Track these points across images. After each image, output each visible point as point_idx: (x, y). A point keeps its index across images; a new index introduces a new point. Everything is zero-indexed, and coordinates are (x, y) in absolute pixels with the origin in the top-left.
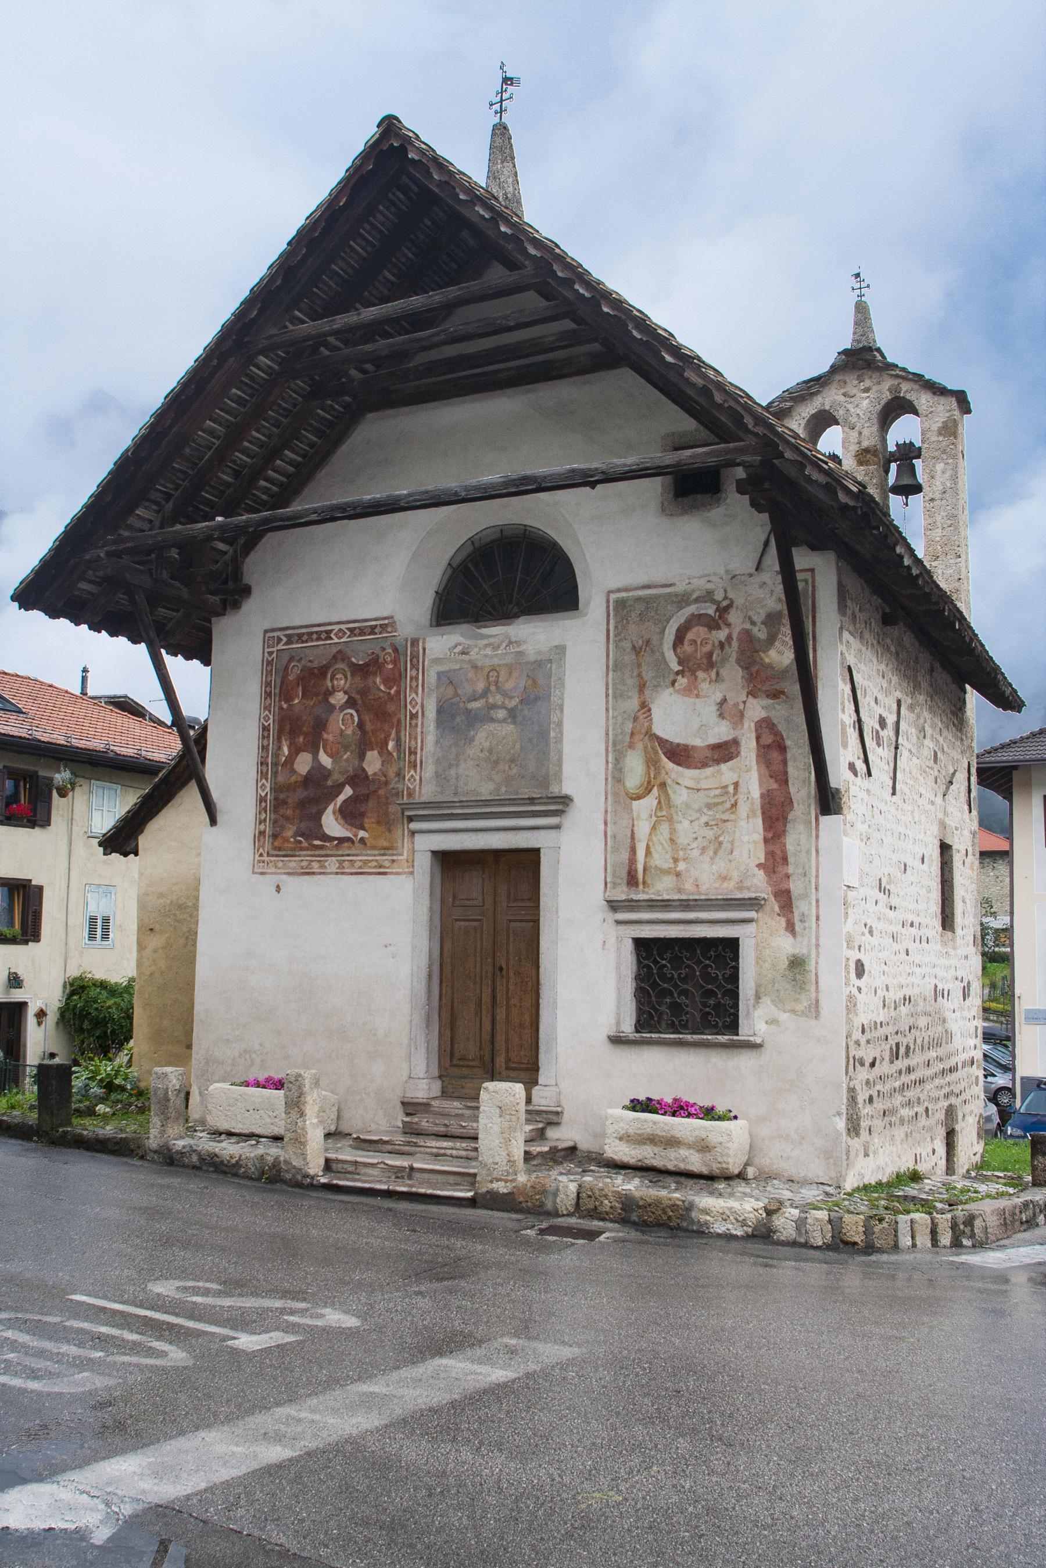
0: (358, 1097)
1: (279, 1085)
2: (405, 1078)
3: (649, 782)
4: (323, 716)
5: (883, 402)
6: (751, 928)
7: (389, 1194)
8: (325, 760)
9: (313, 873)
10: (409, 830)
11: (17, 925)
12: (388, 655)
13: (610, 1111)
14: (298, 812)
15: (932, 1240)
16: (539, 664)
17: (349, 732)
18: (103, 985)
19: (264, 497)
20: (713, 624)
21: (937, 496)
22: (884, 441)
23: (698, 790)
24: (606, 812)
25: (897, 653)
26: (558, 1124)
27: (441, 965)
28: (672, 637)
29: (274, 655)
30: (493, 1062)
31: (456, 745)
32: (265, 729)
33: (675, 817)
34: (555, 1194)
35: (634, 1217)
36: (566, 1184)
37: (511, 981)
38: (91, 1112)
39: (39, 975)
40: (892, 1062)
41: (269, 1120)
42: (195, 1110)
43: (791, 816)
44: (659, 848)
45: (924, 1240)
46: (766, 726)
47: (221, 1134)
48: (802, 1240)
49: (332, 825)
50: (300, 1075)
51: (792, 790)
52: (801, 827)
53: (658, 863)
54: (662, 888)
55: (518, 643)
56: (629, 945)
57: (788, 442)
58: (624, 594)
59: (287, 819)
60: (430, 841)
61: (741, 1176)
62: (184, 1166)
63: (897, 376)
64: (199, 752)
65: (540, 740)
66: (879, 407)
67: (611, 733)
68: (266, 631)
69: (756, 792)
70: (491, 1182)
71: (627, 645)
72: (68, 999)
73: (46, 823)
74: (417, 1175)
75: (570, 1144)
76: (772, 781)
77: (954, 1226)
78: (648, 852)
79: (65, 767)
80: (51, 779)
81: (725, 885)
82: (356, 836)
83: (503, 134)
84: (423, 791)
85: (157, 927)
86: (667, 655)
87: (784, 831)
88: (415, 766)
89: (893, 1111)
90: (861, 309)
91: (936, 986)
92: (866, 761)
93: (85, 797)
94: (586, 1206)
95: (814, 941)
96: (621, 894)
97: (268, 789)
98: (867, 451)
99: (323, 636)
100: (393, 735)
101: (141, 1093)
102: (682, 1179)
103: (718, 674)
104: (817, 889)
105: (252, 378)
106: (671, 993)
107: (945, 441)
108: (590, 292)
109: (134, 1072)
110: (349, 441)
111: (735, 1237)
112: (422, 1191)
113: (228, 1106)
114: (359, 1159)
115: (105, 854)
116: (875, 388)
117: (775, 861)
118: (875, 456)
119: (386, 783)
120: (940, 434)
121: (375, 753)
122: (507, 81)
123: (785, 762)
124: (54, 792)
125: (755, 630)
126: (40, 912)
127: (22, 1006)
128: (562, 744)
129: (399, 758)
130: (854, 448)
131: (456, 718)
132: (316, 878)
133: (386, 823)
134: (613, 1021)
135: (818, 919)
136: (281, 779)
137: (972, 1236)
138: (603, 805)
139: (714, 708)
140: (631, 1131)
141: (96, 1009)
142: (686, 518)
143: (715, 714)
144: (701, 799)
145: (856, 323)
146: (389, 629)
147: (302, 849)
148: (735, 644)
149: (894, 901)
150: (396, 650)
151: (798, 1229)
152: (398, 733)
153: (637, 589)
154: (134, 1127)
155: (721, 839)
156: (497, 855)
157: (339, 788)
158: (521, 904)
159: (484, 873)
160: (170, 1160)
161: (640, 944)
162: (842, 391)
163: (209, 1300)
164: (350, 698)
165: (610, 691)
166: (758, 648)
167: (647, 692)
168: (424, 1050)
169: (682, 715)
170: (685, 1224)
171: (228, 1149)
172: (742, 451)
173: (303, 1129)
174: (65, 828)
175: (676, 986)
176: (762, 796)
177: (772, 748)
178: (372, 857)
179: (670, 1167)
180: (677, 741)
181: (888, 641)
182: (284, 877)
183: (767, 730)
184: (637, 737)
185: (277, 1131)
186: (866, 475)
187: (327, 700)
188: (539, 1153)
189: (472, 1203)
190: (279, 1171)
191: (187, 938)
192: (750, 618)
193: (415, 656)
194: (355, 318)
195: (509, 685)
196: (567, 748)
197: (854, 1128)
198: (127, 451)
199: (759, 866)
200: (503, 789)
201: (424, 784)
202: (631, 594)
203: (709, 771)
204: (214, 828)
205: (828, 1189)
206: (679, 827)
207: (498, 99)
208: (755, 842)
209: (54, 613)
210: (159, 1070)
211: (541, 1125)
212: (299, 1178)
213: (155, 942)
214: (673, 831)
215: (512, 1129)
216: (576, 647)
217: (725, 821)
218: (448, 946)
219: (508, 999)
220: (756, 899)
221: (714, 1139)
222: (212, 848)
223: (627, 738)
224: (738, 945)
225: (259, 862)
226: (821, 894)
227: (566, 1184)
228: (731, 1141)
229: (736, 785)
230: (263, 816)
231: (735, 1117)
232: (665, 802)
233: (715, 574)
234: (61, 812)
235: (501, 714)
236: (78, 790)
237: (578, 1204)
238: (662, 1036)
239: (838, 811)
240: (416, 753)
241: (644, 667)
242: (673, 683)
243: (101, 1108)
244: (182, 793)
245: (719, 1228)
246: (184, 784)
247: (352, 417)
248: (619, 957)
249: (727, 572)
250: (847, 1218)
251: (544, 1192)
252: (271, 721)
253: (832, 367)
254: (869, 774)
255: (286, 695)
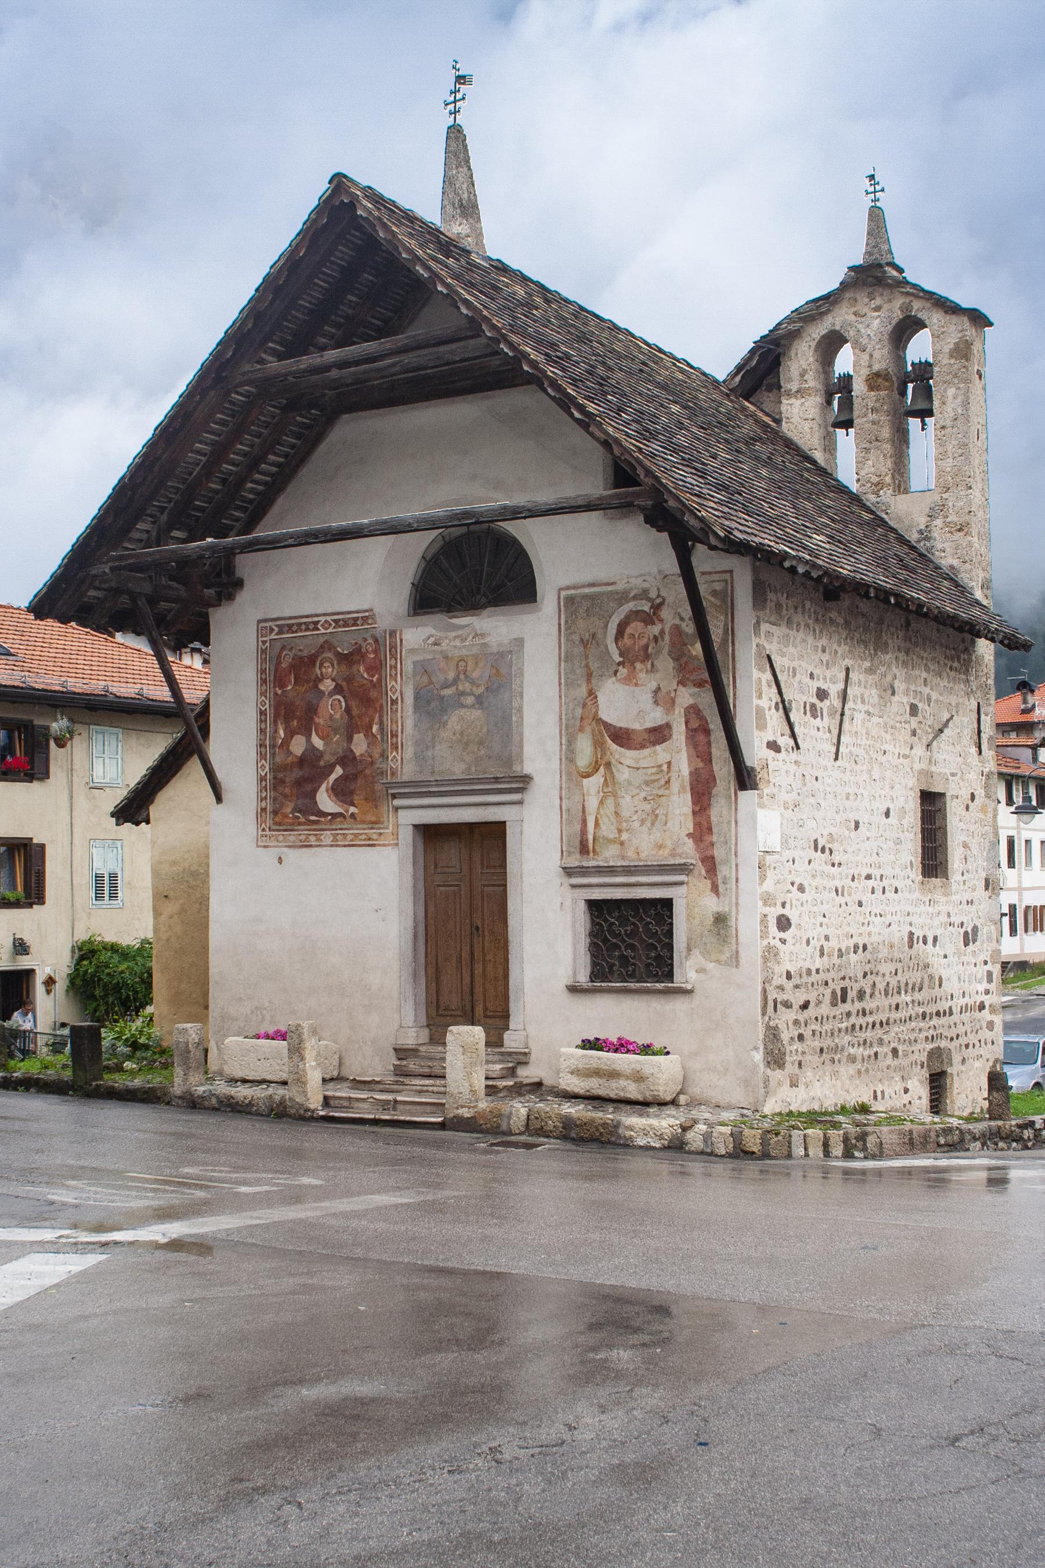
0: (357, 1046)
1: (282, 1036)
2: (396, 1027)
3: (596, 762)
4: (315, 702)
5: (894, 322)
6: (682, 890)
7: (376, 1122)
8: (318, 742)
9: (311, 846)
10: (393, 806)
11: (20, 887)
12: (369, 646)
13: (563, 1050)
14: (295, 790)
15: (824, 1151)
16: (502, 655)
17: (338, 716)
18: (114, 948)
19: (251, 496)
20: (648, 619)
21: (948, 423)
22: (900, 360)
23: (638, 769)
24: (561, 788)
25: (847, 623)
26: (526, 1063)
27: (426, 926)
28: (614, 631)
29: (268, 644)
30: (472, 1011)
31: (432, 728)
32: (262, 713)
33: (619, 793)
34: (509, 1118)
35: (573, 1135)
36: (519, 1109)
37: (487, 938)
38: (119, 1069)
39: (46, 939)
40: (834, 1004)
41: (277, 1067)
42: (213, 1065)
43: (714, 792)
44: (606, 820)
45: (816, 1151)
46: (694, 712)
47: (237, 1081)
48: (709, 1150)
49: (326, 802)
50: (299, 1025)
51: (716, 768)
52: (723, 801)
53: (605, 833)
54: (609, 856)
55: (483, 635)
56: (582, 906)
57: (671, 492)
58: (572, 592)
59: (286, 796)
60: (410, 818)
61: (674, 1102)
62: (205, 1108)
63: (908, 294)
64: (200, 728)
65: (505, 727)
66: (890, 328)
67: (564, 717)
68: (259, 622)
69: (685, 771)
70: (457, 1108)
71: (576, 638)
72: (77, 964)
73: (45, 775)
74: (400, 1107)
75: (537, 1080)
76: (699, 760)
77: (846, 1140)
78: (597, 824)
79: (62, 715)
80: (47, 728)
81: (661, 852)
82: (347, 811)
83: (457, 138)
84: (405, 770)
85: (171, 894)
86: (610, 648)
87: (709, 805)
88: (397, 748)
89: (836, 1049)
90: (876, 218)
91: (911, 934)
92: (793, 735)
93: (85, 745)
94: (536, 1128)
95: (734, 900)
96: (574, 861)
97: (267, 769)
98: (877, 375)
99: (311, 627)
100: (376, 720)
101: (163, 1052)
102: (620, 1105)
103: (652, 665)
104: (736, 855)
105: (232, 403)
106: (618, 947)
107: (956, 364)
108: (513, 351)
109: (155, 1031)
110: (327, 440)
111: (654, 1148)
112: (402, 1118)
113: (242, 1057)
114: (352, 1095)
115: (117, 825)
116: (886, 307)
117: (702, 831)
118: (887, 380)
119: (372, 763)
120: (952, 356)
121: (362, 735)
122: (461, 79)
123: (709, 743)
124: (52, 744)
125: (684, 625)
126: (44, 872)
127: (30, 973)
128: (522, 728)
129: (382, 740)
130: (865, 372)
131: (432, 704)
132: (313, 850)
133: (373, 800)
134: (571, 973)
135: (737, 881)
136: (278, 759)
137: (864, 1149)
138: (558, 782)
139: (651, 695)
140: (580, 1066)
141: (109, 974)
142: (624, 522)
143: (651, 701)
144: (640, 777)
145: (868, 234)
146: (370, 621)
147: (300, 824)
148: (667, 637)
149: (836, 858)
150: (376, 641)
151: (705, 1141)
152: (381, 716)
153: (583, 586)
154: (158, 1079)
155: (657, 812)
156: (471, 827)
157: (331, 768)
158: (492, 871)
159: (460, 842)
160: (193, 1104)
161: (595, 907)
162: (854, 309)
163: (223, 1175)
164: (337, 684)
165: (563, 681)
166: (686, 641)
167: (594, 681)
168: (412, 1002)
169: (624, 702)
170: (613, 1139)
171: (242, 1092)
172: (638, 495)
173: (304, 1070)
174: (65, 780)
175: (623, 941)
176: (691, 774)
177: (698, 731)
178: (362, 830)
179: (613, 1096)
180: (619, 725)
181: (833, 615)
182: (285, 850)
183: (693, 715)
184: (586, 722)
185: (284, 1076)
186: (877, 400)
187: (317, 687)
188: (505, 1087)
189: (442, 1126)
190: (285, 1108)
191: (201, 903)
192: (679, 615)
193: (393, 647)
194: (319, 360)
195: (475, 675)
196: (527, 732)
197: (776, 1059)
198: (123, 477)
199: (689, 835)
200: (473, 769)
201: (404, 764)
202: (579, 591)
203: (646, 752)
204: (220, 805)
205: (745, 1111)
206: (621, 801)
207: (452, 99)
208: (684, 814)
209: (64, 620)
210: (180, 1026)
211: (511, 1065)
212: (302, 1112)
213: (170, 908)
214: (617, 805)
215: (473, 1064)
216: (531, 640)
217: (660, 796)
218: (431, 909)
219: (484, 955)
220: (684, 864)
221: (647, 1071)
222: (220, 821)
223: (578, 722)
224: (672, 905)
225: (262, 836)
226: (740, 860)
227: (519, 1109)
228: (663, 1073)
229: (669, 763)
230: (264, 795)
231: (668, 1053)
232: (610, 780)
233: (649, 574)
234: (60, 763)
235: (470, 700)
236: (77, 739)
237: (527, 1125)
238: (610, 984)
239: (754, 787)
240: (397, 736)
241: (591, 659)
242: (616, 673)
243: (128, 1065)
244: (189, 763)
245: (641, 1142)
246: (190, 755)
247: (329, 419)
248: (574, 917)
249: (659, 572)
250: (747, 1132)
251: (500, 1116)
252: (267, 706)
253: (841, 284)
254: (798, 748)
255: (280, 681)
